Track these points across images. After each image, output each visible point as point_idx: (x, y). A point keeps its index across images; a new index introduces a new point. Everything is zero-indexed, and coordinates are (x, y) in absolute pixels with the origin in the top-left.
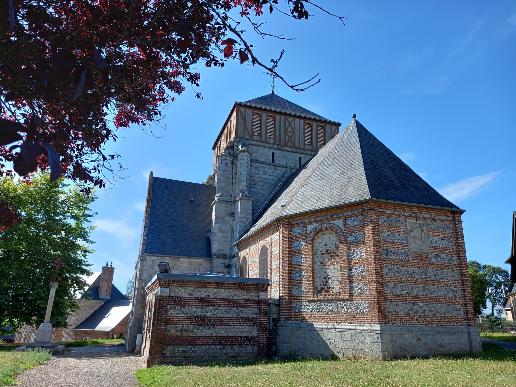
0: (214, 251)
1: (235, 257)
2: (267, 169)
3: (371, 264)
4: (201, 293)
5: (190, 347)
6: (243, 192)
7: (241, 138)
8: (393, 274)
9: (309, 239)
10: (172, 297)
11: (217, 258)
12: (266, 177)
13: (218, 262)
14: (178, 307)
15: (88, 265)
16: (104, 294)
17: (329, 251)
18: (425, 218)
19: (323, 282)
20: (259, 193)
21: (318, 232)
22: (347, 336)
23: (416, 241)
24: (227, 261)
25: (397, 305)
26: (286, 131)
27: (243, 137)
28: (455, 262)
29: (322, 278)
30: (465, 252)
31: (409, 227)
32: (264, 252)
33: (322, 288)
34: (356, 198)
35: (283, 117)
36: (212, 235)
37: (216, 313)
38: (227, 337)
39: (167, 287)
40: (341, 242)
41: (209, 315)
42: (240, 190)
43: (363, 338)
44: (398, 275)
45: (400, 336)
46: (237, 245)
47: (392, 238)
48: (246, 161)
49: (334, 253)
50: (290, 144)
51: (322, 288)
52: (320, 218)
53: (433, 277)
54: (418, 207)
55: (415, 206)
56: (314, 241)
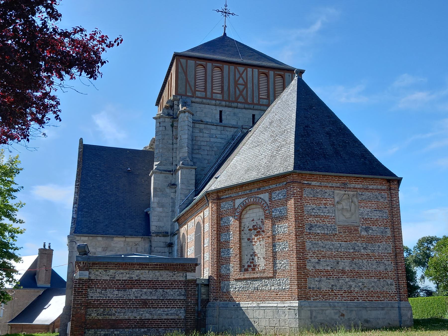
0: (153, 228)
1: (176, 234)
2: (215, 131)
3: (292, 240)
4: (123, 275)
5: (112, 330)
6: (184, 159)
7: (181, 95)
8: (317, 249)
9: (236, 214)
10: (92, 280)
11: (157, 236)
12: (212, 140)
13: (158, 241)
14: (98, 290)
15: (16, 249)
16: (43, 280)
17: (255, 227)
18: (356, 188)
19: (250, 259)
20: (205, 159)
21: (245, 207)
22: (270, 314)
23: (345, 214)
24: (168, 240)
25: (320, 281)
26: (236, 84)
27: (184, 93)
28: (389, 233)
29: (249, 256)
30: (400, 223)
31: (337, 199)
32: (198, 228)
33: (247, 266)
34: (281, 170)
35: (232, 67)
36: (151, 209)
37: (139, 295)
38: (152, 319)
39: (87, 269)
40: (266, 218)
41: (132, 297)
42: (180, 158)
43: (283, 315)
44: (322, 250)
45: (320, 312)
46: (177, 220)
47: (318, 211)
48: (186, 123)
49: (261, 228)
50: (241, 99)
51: (249, 266)
52: (248, 192)
53: (363, 251)
54: (347, 177)
55: (344, 177)
56: (242, 216)
